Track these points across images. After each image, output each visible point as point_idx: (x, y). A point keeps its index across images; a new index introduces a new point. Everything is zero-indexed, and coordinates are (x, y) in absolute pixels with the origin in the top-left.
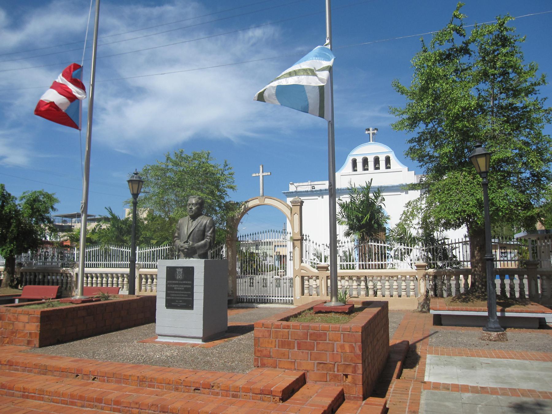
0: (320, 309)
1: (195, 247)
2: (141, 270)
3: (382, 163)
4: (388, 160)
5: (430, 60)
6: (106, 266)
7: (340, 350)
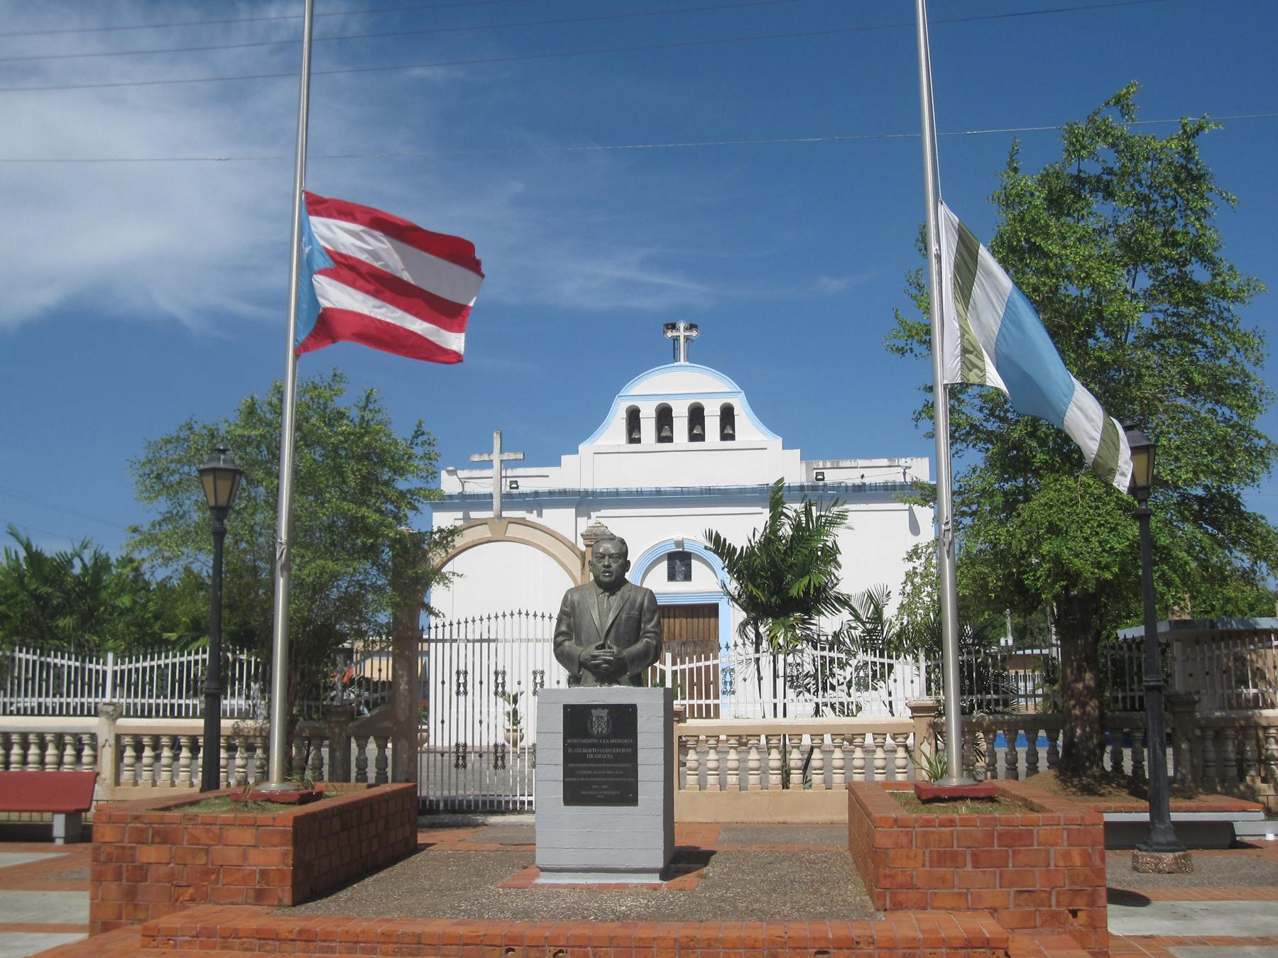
0: (938, 793)
1: (623, 659)
2: (122, 722)
3: (712, 425)
4: (727, 415)
5: (1065, 247)
6: (60, 712)
7: (1061, 863)
